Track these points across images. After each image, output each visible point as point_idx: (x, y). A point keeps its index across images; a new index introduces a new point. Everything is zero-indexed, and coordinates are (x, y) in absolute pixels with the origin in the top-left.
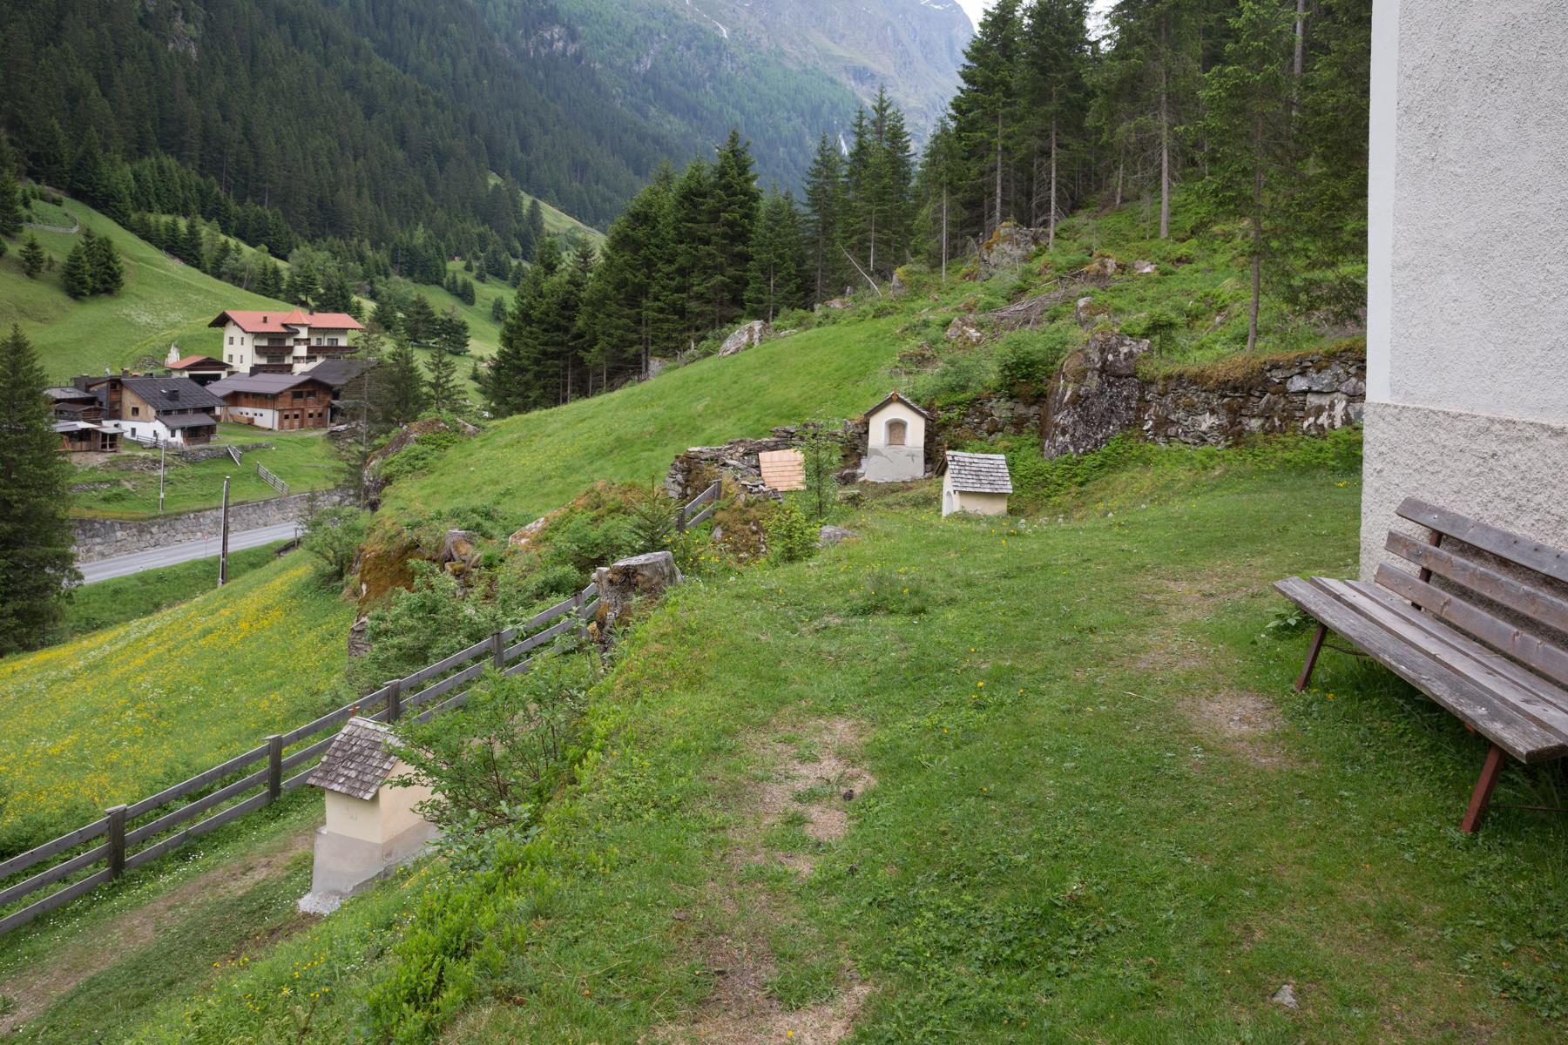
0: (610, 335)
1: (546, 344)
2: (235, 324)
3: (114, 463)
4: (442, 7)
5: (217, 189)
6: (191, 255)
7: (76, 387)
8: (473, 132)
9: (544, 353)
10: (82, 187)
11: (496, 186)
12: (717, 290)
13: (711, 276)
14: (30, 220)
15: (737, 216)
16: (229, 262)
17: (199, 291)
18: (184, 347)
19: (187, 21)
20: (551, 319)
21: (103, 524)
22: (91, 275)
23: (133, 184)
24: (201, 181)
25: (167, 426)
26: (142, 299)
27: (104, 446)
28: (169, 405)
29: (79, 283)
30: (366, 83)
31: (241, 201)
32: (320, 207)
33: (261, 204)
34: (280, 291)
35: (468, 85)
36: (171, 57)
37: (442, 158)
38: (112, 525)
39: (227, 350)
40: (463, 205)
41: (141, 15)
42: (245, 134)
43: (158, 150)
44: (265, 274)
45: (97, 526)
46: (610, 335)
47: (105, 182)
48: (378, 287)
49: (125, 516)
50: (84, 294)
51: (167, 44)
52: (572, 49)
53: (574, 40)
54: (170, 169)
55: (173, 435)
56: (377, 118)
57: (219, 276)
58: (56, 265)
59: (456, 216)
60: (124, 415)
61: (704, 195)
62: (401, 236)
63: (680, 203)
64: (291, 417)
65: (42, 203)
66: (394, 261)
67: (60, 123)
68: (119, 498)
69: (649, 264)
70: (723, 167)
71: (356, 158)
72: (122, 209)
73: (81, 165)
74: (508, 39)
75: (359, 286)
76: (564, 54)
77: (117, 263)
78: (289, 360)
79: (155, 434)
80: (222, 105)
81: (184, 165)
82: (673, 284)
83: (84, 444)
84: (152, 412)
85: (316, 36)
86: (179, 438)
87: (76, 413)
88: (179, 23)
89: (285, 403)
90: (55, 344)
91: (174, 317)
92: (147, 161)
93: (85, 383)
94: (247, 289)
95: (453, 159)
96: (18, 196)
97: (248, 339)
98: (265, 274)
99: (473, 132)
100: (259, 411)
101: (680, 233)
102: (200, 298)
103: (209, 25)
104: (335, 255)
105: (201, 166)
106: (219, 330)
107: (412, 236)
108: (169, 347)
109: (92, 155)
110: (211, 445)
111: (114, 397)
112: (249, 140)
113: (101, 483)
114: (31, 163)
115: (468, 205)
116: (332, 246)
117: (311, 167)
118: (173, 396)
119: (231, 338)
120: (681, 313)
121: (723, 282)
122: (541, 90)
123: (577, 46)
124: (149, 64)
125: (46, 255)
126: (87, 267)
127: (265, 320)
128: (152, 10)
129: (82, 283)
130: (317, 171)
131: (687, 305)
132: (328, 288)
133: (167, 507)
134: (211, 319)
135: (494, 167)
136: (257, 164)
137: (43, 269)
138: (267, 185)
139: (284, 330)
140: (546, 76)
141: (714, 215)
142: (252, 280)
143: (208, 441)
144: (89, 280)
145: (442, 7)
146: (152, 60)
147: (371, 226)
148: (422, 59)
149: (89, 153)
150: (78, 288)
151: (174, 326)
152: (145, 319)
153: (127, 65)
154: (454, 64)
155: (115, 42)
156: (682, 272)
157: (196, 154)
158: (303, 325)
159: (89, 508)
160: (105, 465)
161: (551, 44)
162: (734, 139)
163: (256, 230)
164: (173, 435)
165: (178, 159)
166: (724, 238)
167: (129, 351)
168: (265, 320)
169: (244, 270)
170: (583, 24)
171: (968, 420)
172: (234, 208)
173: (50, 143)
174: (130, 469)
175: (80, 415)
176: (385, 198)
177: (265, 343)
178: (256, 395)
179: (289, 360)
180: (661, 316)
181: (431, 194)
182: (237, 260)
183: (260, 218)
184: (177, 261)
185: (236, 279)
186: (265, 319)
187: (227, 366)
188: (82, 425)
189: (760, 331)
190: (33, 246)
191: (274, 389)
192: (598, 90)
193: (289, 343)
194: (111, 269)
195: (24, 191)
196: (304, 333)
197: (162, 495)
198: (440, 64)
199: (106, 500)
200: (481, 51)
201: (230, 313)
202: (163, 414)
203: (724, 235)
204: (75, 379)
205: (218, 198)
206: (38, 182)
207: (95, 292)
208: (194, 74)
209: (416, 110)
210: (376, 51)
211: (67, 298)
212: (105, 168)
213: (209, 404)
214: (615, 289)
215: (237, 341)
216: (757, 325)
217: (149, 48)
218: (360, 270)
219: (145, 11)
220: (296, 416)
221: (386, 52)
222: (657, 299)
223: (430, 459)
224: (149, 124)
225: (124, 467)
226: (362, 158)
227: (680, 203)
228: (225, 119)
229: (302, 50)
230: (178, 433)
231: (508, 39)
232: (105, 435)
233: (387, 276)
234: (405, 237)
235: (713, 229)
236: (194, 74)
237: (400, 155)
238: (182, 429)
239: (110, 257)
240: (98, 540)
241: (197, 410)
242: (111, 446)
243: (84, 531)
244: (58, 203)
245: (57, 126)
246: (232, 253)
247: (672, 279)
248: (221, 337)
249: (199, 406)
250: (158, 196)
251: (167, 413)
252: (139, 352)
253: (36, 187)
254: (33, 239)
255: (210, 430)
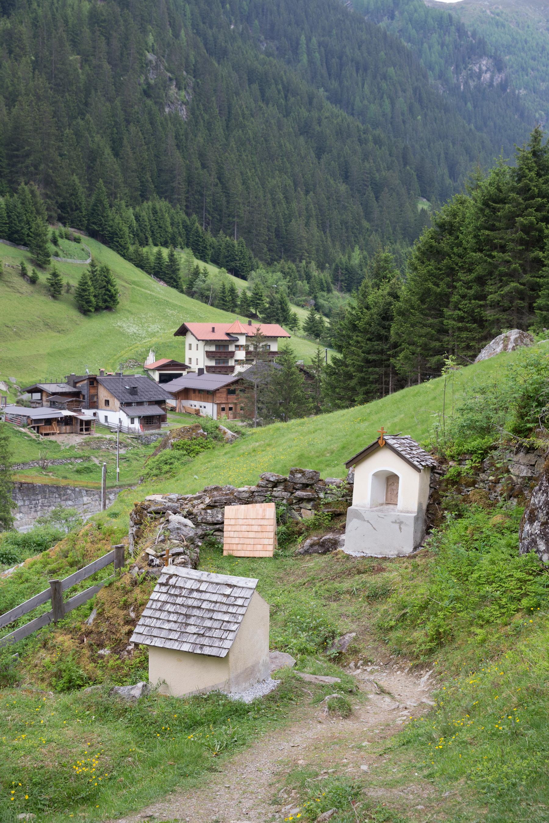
0: (413, 344)
1: (369, 353)
2: (192, 334)
3: (87, 443)
4: (382, 53)
5: (197, 224)
6: (171, 278)
7: (68, 383)
8: (405, 164)
9: (367, 361)
10: (96, 227)
11: (423, 210)
12: (510, 296)
13: (506, 284)
14: (57, 255)
15: (533, 219)
16: (199, 284)
17: (174, 306)
18: (158, 352)
19: (180, 89)
20: (372, 329)
21: (74, 490)
22: (95, 296)
23: (135, 224)
24: (186, 218)
25: (128, 415)
26: (132, 314)
27: (81, 430)
28: (129, 398)
29: (87, 302)
30: (318, 128)
31: (215, 233)
32: (277, 236)
33: (231, 235)
34: (236, 306)
35: (404, 122)
36: (166, 119)
37: (377, 188)
38: (80, 491)
39: (188, 354)
40: (394, 229)
41: (145, 87)
42: (219, 178)
43: (155, 195)
44: (223, 292)
45: (69, 492)
46: (413, 344)
47: (111, 223)
48: (321, 301)
49: (90, 485)
50: (90, 311)
51: (164, 109)
52: (498, 79)
53: (500, 70)
54: (161, 210)
55: (132, 422)
56: (325, 157)
57: (191, 294)
58: (73, 288)
59: (388, 238)
60: (100, 406)
61: (503, 201)
62: (341, 258)
63: (482, 210)
64: (227, 409)
65: (67, 241)
66: (336, 279)
67: (80, 178)
68: (88, 470)
69: (451, 272)
70: (521, 169)
71: (307, 192)
72: (122, 243)
73: (94, 210)
74: (441, 76)
75: (305, 301)
76: (491, 85)
77: (114, 286)
78: (231, 363)
79: (120, 421)
80: (202, 156)
81: (174, 206)
82: (472, 292)
83: (68, 427)
84: (117, 404)
85: (279, 92)
86: (137, 425)
87: (62, 404)
88: (173, 90)
89: (222, 398)
90: (68, 349)
91: (154, 328)
92: (145, 204)
93: (74, 381)
94: (212, 305)
95: (386, 189)
96: (50, 236)
97: (201, 344)
98: (223, 292)
99: (405, 164)
100: (203, 404)
101: (479, 242)
102: (175, 313)
103: (197, 90)
104: (285, 274)
105: (187, 207)
106: (180, 338)
107: (350, 258)
108: (148, 351)
109: (101, 202)
110: (161, 431)
111: (93, 391)
112: (221, 182)
113: (76, 458)
114: (59, 211)
115: (398, 228)
116: (283, 268)
117: (269, 202)
118: (133, 391)
119: (190, 345)
120: (481, 322)
121: (516, 290)
122: (469, 122)
123: (503, 75)
124: (149, 126)
125: (64, 282)
126: (92, 289)
127: (213, 330)
128: (152, 82)
129: (89, 302)
130: (274, 206)
131: (484, 313)
132: (271, 303)
133: (122, 479)
134: (176, 330)
135: (425, 195)
136: (228, 202)
137: (63, 292)
138: (236, 219)
139: (227, 338)
140: (475, 107)
141: (511, 219)
142: (215, 298)
143: (159, 427)
144: (93, 299)
145: (382, 53)
146: (151, 123)
147: (317, 250)
148: (366, 102)
149: (99, 201)
150: (86, 306)
151: (153, 335)
152: (133, 329)
153: (133, 128)
154: (393, 104)
155: (125, 111)
156: (481, 281)
157: (183, 197)
158: (242, 334)
159: (65, 478)
160: (81, 445)
161: (479, 77)
162: (536, 139)
163: (227, 257)
164: (132, 422)
165: (170, 202)
166: (521, 244)
167: (119, 355)
168: (213, 330)
169: (208, 290)
170: (510, 53)
171: (482, 476)
172: (210, 238)
173: (72, 195)
174: (99, 448)
175: (66, 406)
176: (330, 226)
177: (213, 349)
178: (200, 391)
179: (231, 363)
180: (460, 325)
181: (369, 220)
182: (204, 281)
183: (229, 246)
184: (162, 283)
185: (204, 297)
186: (213, 328)
187: (187, 367)
188: (66, 413)
189: (516, 340)
190: (55, 275)
191: (212, 387)
192: (522, 116)
193: (232, 348)
194: (110, 291)
195: (54, 233)
196: (242, 341)
197: (118, 470)
198: (381, 106)
199: (78, 472)
200: (415, 90)
201: (189, 325)
202: (126, 405)
203: (521, 242)
204: (68, 377)
205: (197, 232)
206: (64, 224)
207: (98, 309)
208: (182, 132)
209: (358, 148)
210: (328, 98)
211: (79, 314)
212: (110, 213)
213: (161, 398)
214: (419, 299)
215: (194, 347)
216: (514, 334)
217: (149, 113)
218: (307, 287)
219: (148, 84)
220: (231, 409)
221: (335, 99)
222: (456, 308)
223: (176, 464)
224: (148, 176)
225: (95, 446)
226: (311, 193)
227: (482, 210)
228: (204, 166)
229: (267, 104)
230: (136, 421)
231: (441, 76)
232: (82, 421)
233: (329, 291)
234: (344, 259)
235: (509, 235)
236: (182, 132)
237: (343, 188)
238: (139, 417)
239: (109, 282)
240: (70, 503)
241: (151, 403)
242: (87, 430)
243: (60, 495)
244: (77, 240)
245: (77, 181)
246: (201, 276)
247: (470, 288)
248: (183, 343)
249: (152, 399)
250: (153, 232)
251: (129, 404)
252: (126, 356)
253: (63, 229)
254: (55, 269)
255: (162, 419)
